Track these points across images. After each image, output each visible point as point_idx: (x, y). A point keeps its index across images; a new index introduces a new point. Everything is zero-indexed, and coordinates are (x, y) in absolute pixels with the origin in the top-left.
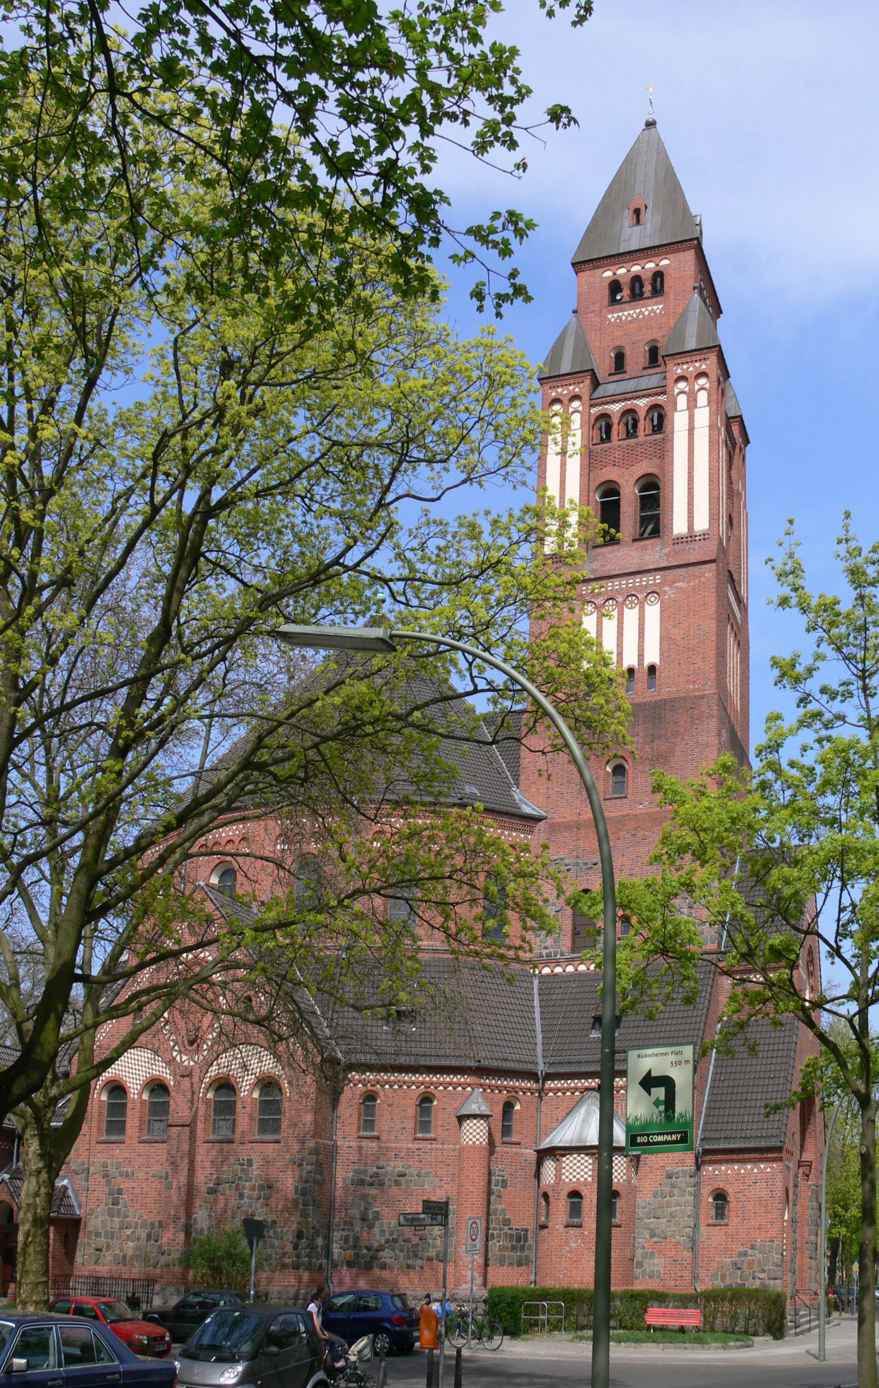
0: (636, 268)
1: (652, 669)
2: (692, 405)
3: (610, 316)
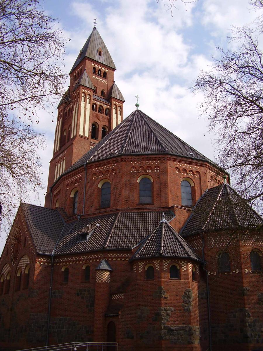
3: (93, 76)
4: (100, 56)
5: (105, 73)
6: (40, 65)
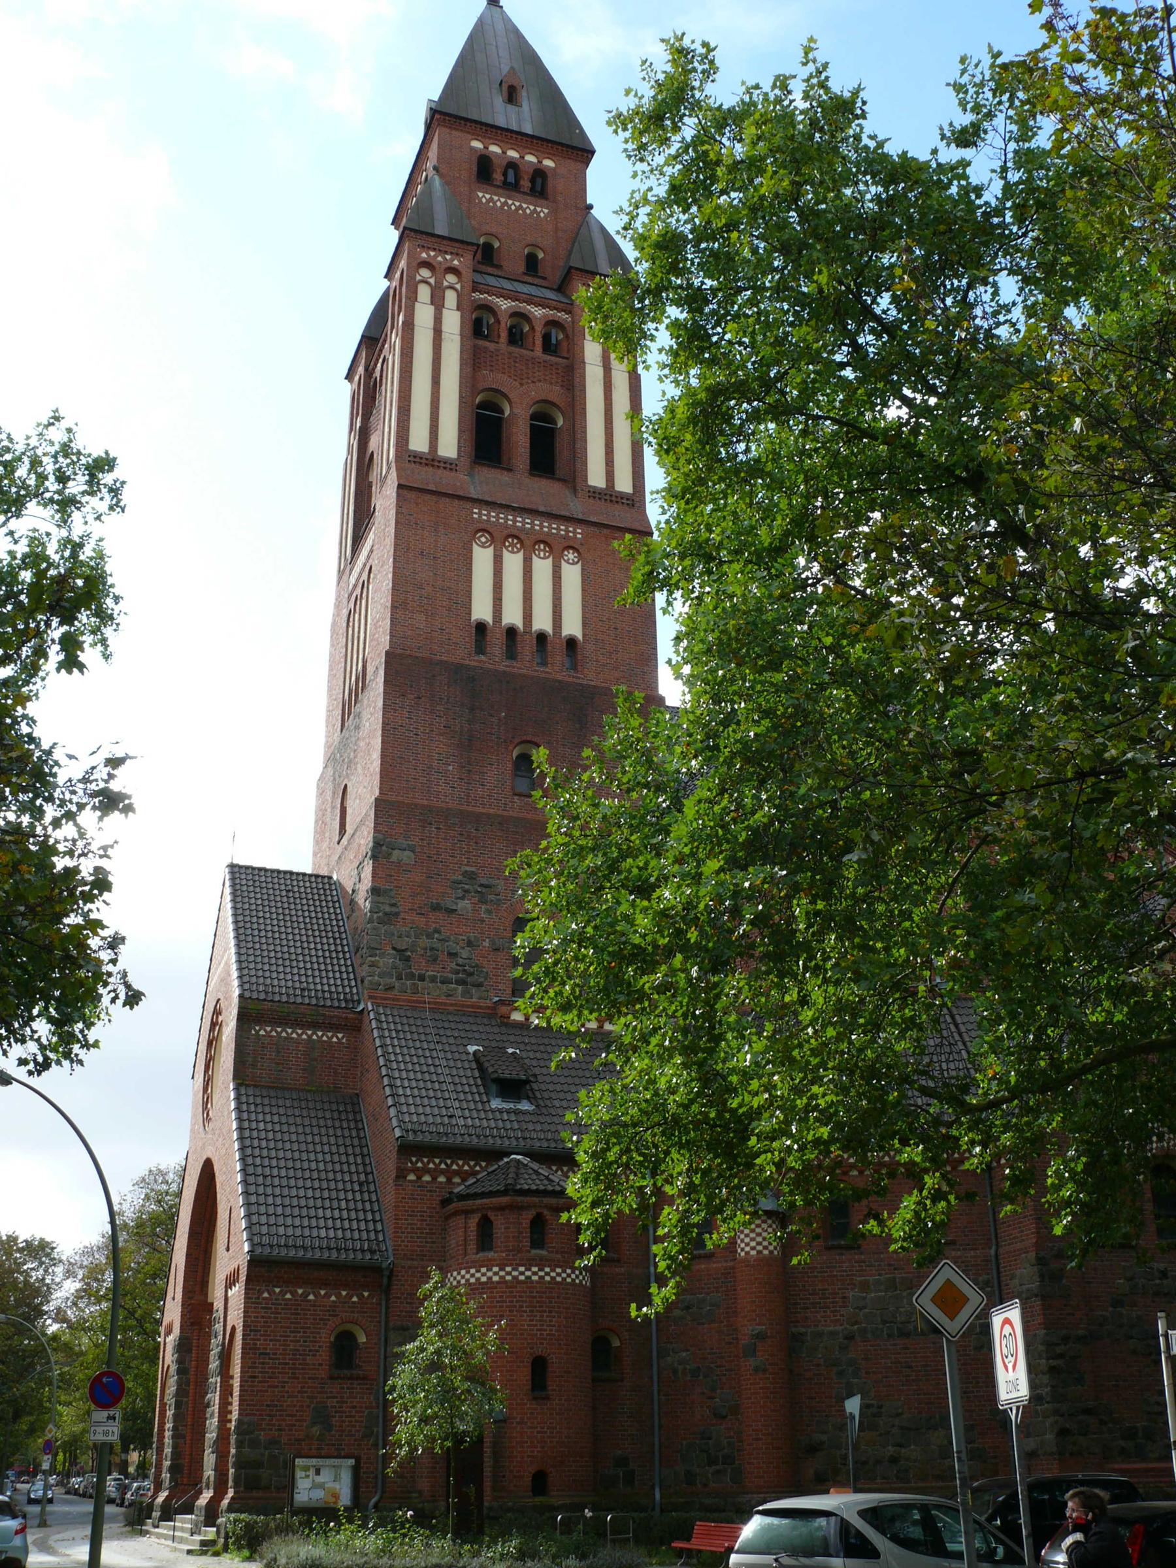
0: (495, 149)
1: (571, 642)
2: (437, 302)
3: (480, 194)
4: (509, 106)
5: (539, 174)
6: (626, 219)
